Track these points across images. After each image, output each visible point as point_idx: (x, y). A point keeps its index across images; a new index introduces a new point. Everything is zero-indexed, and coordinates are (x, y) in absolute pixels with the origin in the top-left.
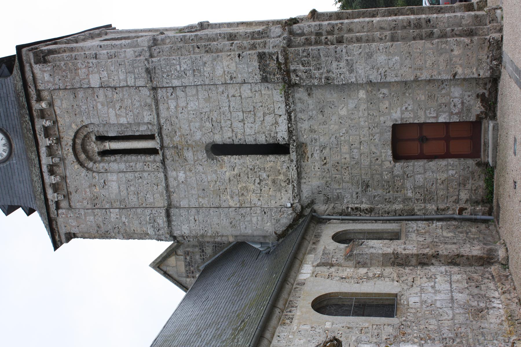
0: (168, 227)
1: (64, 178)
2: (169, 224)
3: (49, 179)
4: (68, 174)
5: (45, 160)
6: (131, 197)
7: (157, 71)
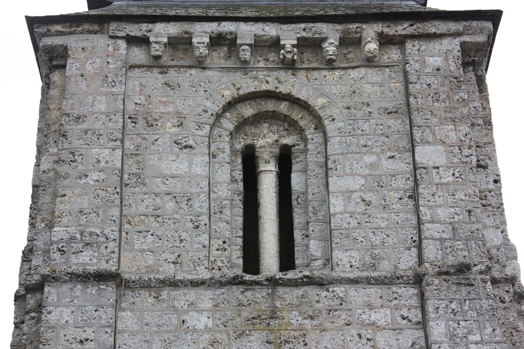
0: (72, 274)
1: (200, 64)
2: (79, 276)
3: (201, 33)
4: (208, 73)
5: (246, 32)
6: (149, 200)
7: (464, 290)
